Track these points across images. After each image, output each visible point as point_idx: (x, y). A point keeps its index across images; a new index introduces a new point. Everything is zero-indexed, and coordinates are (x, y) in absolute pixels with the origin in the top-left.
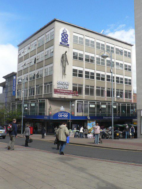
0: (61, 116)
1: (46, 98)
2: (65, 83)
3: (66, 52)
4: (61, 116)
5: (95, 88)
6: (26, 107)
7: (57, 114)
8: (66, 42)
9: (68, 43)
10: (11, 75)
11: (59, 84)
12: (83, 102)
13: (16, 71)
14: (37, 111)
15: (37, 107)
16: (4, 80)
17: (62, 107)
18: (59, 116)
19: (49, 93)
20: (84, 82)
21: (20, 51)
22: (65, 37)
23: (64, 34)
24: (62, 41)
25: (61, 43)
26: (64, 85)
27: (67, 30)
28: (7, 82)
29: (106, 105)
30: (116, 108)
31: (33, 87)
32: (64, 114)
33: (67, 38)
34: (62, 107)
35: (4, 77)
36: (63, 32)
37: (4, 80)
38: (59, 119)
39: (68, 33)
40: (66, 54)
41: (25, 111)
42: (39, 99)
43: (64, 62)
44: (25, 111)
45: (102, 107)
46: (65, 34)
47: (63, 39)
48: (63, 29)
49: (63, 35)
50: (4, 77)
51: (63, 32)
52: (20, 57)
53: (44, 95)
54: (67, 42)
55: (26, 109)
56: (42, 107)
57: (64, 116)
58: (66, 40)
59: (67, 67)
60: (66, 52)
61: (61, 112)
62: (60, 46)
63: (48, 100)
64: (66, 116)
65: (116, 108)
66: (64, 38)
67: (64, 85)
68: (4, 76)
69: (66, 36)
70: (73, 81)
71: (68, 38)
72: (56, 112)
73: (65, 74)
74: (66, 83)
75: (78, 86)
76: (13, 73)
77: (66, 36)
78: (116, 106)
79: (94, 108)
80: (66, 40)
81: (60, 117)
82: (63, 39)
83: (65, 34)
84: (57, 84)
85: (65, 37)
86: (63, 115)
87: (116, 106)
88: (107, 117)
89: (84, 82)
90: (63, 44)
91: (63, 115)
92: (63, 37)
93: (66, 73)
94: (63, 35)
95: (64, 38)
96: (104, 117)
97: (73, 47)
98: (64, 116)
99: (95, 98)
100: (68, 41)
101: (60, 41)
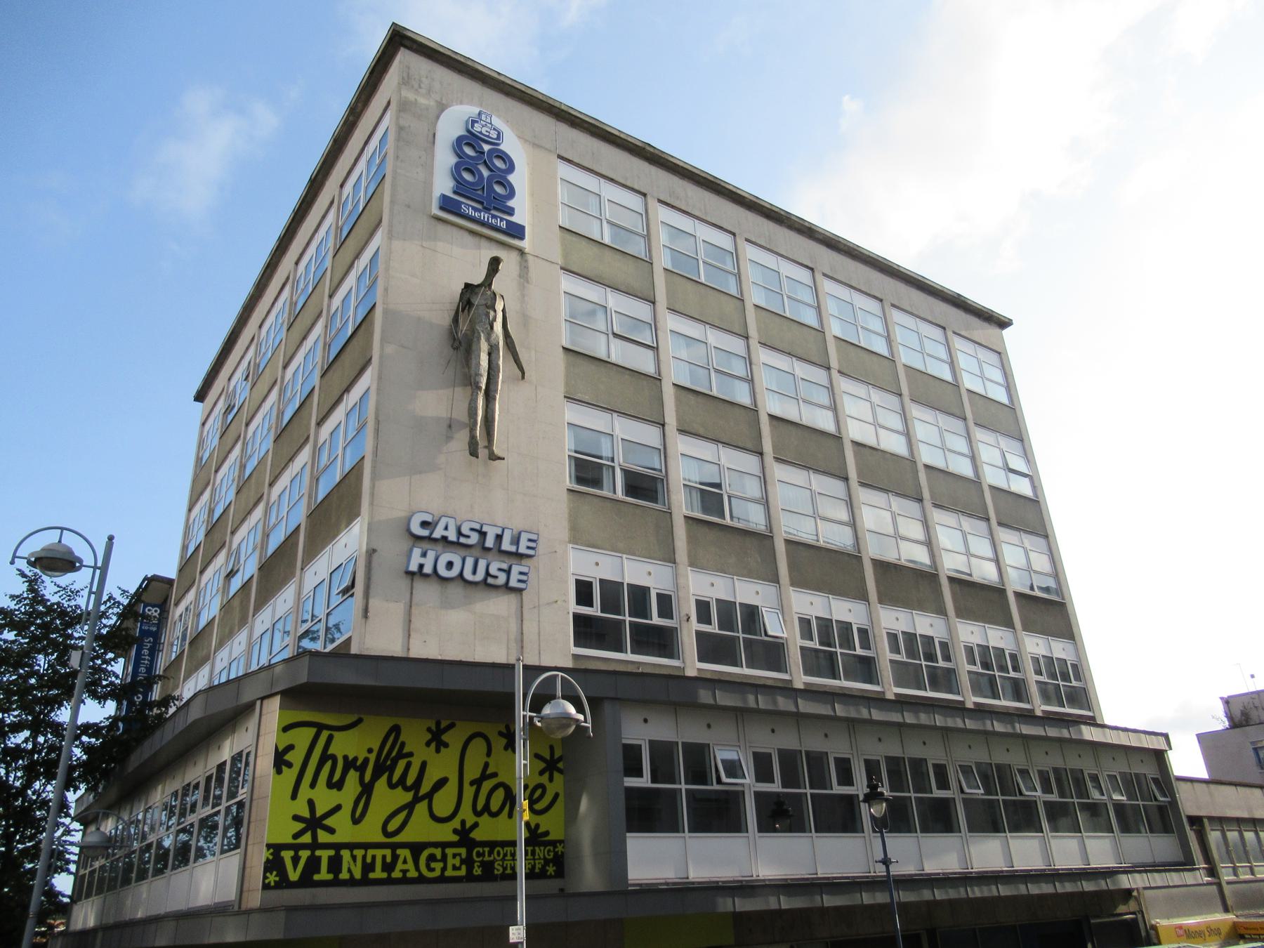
2: (491, 534)
62: (441, 228)
74: (499, 538)
97: (566, 255)
101: (443, 185)
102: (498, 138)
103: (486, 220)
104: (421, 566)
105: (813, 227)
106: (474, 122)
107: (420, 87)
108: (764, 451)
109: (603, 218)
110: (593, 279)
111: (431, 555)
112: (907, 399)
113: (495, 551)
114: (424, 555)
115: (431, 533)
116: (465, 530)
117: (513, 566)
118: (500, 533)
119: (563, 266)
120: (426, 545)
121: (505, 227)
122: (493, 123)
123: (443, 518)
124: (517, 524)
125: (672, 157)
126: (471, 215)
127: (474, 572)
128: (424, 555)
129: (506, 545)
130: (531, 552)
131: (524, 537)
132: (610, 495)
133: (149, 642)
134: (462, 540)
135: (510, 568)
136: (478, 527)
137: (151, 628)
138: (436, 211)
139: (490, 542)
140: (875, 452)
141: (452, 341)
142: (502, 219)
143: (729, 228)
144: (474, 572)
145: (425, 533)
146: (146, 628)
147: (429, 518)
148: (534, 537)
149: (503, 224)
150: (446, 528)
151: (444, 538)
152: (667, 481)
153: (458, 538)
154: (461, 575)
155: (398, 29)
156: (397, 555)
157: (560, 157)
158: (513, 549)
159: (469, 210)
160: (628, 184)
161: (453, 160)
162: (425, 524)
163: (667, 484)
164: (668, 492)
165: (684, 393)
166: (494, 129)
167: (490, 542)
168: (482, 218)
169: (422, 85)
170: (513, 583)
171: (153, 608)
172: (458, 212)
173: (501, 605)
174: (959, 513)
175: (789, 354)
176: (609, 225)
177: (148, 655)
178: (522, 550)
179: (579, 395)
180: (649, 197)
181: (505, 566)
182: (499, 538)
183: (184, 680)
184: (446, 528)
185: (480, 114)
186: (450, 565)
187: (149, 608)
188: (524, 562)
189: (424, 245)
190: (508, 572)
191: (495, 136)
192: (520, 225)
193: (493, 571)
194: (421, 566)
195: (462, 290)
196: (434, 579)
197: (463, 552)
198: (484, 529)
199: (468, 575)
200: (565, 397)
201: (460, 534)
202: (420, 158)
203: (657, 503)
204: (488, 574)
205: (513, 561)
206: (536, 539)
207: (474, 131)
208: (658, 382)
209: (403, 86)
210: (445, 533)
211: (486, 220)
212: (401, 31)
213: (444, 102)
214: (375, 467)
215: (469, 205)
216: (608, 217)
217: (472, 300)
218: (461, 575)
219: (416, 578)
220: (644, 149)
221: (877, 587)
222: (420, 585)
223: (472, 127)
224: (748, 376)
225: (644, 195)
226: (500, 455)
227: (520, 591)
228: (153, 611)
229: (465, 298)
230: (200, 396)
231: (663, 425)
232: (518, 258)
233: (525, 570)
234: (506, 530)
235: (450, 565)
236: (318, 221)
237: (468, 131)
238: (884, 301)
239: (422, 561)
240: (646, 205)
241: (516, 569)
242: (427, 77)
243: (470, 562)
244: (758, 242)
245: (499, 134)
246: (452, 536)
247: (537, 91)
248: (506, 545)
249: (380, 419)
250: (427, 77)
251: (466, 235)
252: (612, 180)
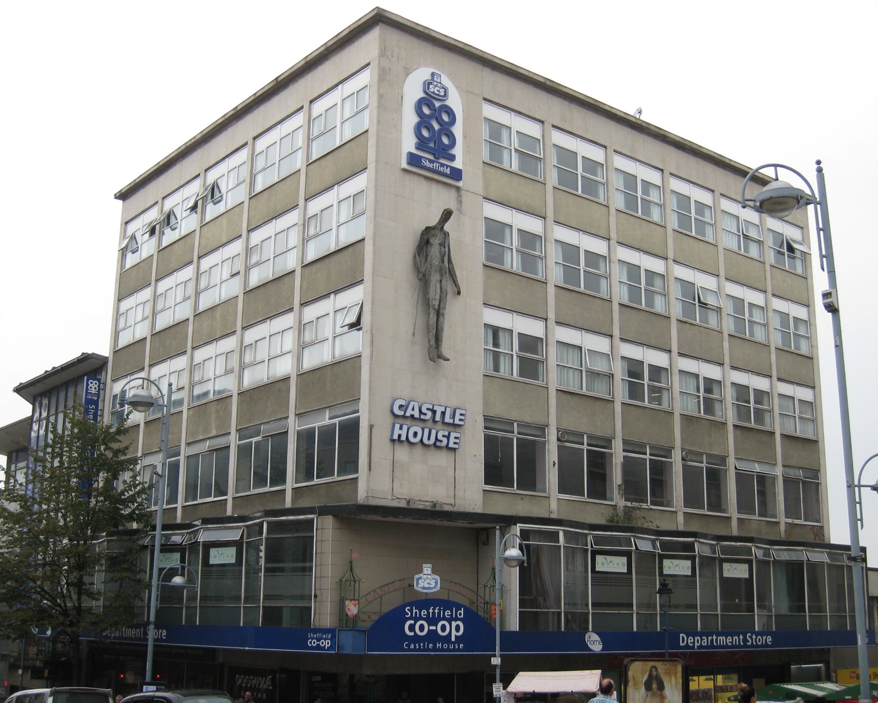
0: (423, 628)
1: (323, 511)
2: (439, 410)
3: (447, 215)
4: (422, 628)
5: (618, 454)
6: (173, 572)
7: (396, 618)
8: (444, 152)
9: (458, 164)
10: (65, 376)
11: (404, 417)
12: (554, 536)
13: (104, 349)
14: (251, 597)
15: (253, 572)
16: (23, 409)
17: (427, 569)
18: (412, 628)
19: (336, 478)
20: (553, 410)
21: (132, 228)
22: (436, 127)
23: (430, 106)
24: (422, 144)
25: (413, 160)
26: (435, 422)
27: (446, 81)
28: (40, 420)
29: (749, 562)
30: (747, 576)
31: (220, 442)
32: (440, 619)
33: (446, 129)
34: (427, 569)
35: (20, 390)
36: (423, 95)
37: (23, 409)
38: (411, 650)
39: (455, 101)
40: (447, 227)
41: (170, 595)
42: (268, 513)
43: (435, 278)
44: (170, 595)
45: (666, 571)
46: (437, 104)
47: (425, 133)
48: (422, 74)
49: (426, 111)
50: (20, 390)
51: (423, 95)
52: (131, 260)
53: (295, 490)
54: (452, 158)
55: (178, 580)
56: (281, 570)
57: (443, 628)
58: (445, 140)
59: (454, 311)
60: (447, 215)
61: (425, 602)
62: (407, 177)
63: (329, 521)
64: (455, 629)
65: (747, 576)
66: (429, 128)
67: (430, 424)
68: (26, 378)
69: (445, 118)
70: (486, 404)
71: (457, 130)
72: (389, 604)
73: (440, 356)
74: (443, 413)
75: (515, 437)
76: (85, 358)
77: (445, 118)
78: (688, 563)
79: (622, 580)
80: (445, 140)
81: (416, 639)
82: (425, 133)
83: (437, 104)
84: (389, 419)
85: (436, 127)
86: (433, 621)
87: (688, 563)
88: (701, 635)
89: (553, 410)
90: (428, 164)
91: (433, 621)
92: (423, 122)
93: (445, 350)
94: (426, 111)
95: (429, 128)
96: (684, 640)
97: (486, 186)
98: (443, 628)
99: (554, 505)
100: (458, 151)
101: (409, 144)
102: (445, 95)
103: (437, 169)
104: (400, 436)
105: (666, 134)
106: (430, 84)
107: (392, 56)
108: (613, 334)
109: (512, 148)
110: (505, 204)
111: (405, 428)
112: (722, 279)
113: (440, 423)
114: (401, 428)
115: (405, 413)
116: (424, 410)
117: (451, 433)
118: (444, 410)
119: (485, 196)
120: (401, 421)
121: (449, 173)
122: (442, 82)
123: (412, 402)
124: (454, 403)
125: (566, 87)
126: (428, 167)
127: (429, 438)
128: (401, 428)
129: (447, 419)
130: (461, 423)
131: (458, 412)
132: (507, 375)
133: (93, 409)
134: (422, 417)
135: (449, 434)
136: (431, 407)
137: (93, 398)
138: (404, 165)
139: (438, 417)
140: (692, 327)
141: (417, 273)
142: (447, 166)
143: (602, 143)
144: (429, 438)
145: (401, 413)
146: (90, 397)
147: (403, 403)
148: (463, 412)
149: (448, 171)
150: (413, 409)
151: (412, 416)
152: (546, 363)
153: (420, 416)
154: (421, 441)
155: (380, 11)
156: (386, 428)
157: (485, 99)
158: (451, 421)
159: (426, 162)
160: (531, 115)
161: (415, 119)
162: (401, 406)
163: (547, 365)
164: (547, 371)
165: (562, 291)
166: (443, 88)
167: (438, 417)
168: (435, 168)
169: (394, 55)
170: (451, 445)
171: (94, 381)
172: (420, 166)
173: (442, 459)
174: (750, 373)
175: (638, 249)
176: (517, 154)
177: (93, 419)
178: (457, 422)
179: (493, 301)
180: (546, 123)
181: (446, 433)
182: (443, 413)
183: (592, 651)
184: (413, 409)
185: (433, 74)
186: (415, 434)
187: (98, 384)
188: (457, 430)
189: (397, 194)
190: (448, 437)
191: (442, 94)
192: (459, 169)
193: (440, 437)
194: (400, 436)
195: (423, 231)
196: (406, 443)
197: (422, 424)
198: (435, 409)
199: (425, 441)
200: (484, 304)
201: (421, 412)
202: (393, 119)
203: (538, 380)
204: (436, 439)
205: (450, 429)
206: (465, 413)
207: (428, 92)
208: (544, 285)
209: (382, 58)
210: (413, 413)
211: (437, 169)
212: (382, 13)
213: (408, 66)
214: (371, 368)
215: (427, 158)
216: (516, 147)
217: (431, 241)
218: (421, 441)
219: (397, 443)
220: (545, 83)
221: (682, 435)
222: (397, 446)
223: (429, 88)
224: (607, 273)
225: (542, 122)
226: (448, 357)
227: (454, 449)
228: (94, 384)
229: (425, 238)
230: (124, 196)
231: (546, 320)
232: (456, 194)
233: (458, 435)
234: (447, 408)
235: (415, 434)
236: (282, 117)
237: (425, 92)
238: (715, 192)
239: (400, 432)
240: (543, 130)
241: (453, 435)
242: (397, 46)
243: (426, 431)
244: (624, 152)
245: (445, 92)
246: (417, 415)
247: (471, 46)
248: (447, 419)
249: (373, 333)
250: (397, 46)
251: (422, 180)
252: (520, 113)
